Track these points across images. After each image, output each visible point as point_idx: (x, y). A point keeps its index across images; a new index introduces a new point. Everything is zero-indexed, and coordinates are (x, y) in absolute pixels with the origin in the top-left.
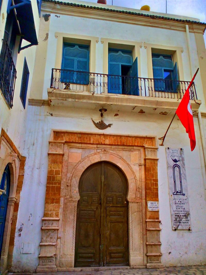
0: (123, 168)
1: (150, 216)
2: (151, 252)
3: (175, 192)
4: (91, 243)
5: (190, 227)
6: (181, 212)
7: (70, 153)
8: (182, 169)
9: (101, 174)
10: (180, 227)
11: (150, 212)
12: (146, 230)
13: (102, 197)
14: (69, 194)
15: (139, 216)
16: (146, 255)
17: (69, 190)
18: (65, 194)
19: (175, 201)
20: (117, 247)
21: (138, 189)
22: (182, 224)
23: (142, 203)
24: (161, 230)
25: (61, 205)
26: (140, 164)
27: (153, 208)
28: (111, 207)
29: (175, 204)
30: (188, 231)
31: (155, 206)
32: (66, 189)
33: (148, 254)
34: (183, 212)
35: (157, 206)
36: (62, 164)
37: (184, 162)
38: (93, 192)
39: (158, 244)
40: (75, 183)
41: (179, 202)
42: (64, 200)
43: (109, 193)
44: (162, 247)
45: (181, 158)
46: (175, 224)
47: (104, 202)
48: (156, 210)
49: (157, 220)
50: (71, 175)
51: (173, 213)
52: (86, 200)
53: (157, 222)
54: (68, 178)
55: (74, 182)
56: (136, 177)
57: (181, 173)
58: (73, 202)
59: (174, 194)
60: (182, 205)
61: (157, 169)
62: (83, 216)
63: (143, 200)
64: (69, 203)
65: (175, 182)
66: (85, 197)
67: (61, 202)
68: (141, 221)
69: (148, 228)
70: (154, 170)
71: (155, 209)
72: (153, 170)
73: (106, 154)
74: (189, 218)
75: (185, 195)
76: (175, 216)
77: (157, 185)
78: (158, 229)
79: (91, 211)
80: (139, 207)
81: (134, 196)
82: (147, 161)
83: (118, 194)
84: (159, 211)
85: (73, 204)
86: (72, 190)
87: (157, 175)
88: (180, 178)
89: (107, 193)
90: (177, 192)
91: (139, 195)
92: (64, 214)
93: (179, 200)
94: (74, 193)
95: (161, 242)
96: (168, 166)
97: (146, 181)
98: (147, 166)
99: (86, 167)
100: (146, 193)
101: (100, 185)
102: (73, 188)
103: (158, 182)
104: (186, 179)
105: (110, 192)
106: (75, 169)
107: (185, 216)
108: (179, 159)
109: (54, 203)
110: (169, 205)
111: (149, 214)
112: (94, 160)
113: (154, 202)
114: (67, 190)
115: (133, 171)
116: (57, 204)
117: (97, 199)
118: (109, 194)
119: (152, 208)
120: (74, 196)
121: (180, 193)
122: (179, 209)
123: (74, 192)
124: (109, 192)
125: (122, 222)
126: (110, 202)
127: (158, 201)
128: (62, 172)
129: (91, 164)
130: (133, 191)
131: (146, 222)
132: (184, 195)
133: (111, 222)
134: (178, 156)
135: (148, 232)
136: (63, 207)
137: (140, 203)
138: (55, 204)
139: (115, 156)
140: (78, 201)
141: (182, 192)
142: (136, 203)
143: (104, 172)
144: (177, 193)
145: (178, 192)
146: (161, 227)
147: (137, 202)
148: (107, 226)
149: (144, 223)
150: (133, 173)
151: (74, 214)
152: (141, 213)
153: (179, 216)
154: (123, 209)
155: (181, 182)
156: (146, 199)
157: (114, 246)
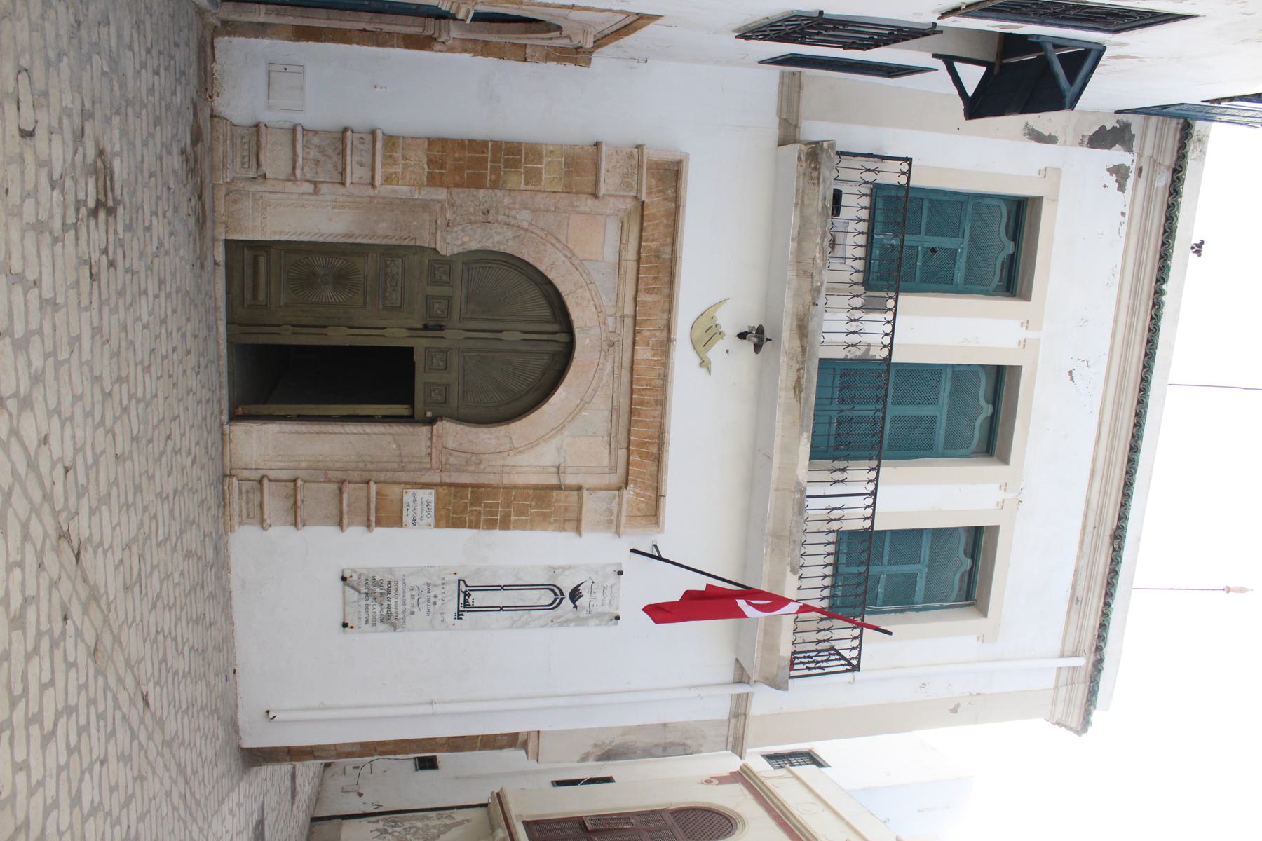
6: (400, 600)
12: (343, 482)
16: (263, 477)
19: (435, 586)
22: (363, 603)
29: (429, 585)
33: (265, 481)
34: (400, 608)
40: (497, 238)
42: (439, 201)
45: (583, 614)
46: (363, 578)
48: (407, 519)
50: (525, 225)
51: (398, 576)
53: (369, 520)
54: (513, 213)
55: (499, 234)
60: (424, 606)
65: (502, 588)
67: (432, 189)
68: (370, 466)
69: (348, 488)
74: (381, 626)
82: (575, 493)
88: (516, 608)
90: (467, 594)
92: (391, 203)
98: (555, 493)
100: (464, 486)
102: (479, 231)
107: (389, 615)
112: (577, 304)
122: (413, 596)
127: (437, 526)
131: (368, 483)
135: (334, 486)
137: (428, 466)
147: (430, 454)
152: (395, 465)
156: (441, 485)
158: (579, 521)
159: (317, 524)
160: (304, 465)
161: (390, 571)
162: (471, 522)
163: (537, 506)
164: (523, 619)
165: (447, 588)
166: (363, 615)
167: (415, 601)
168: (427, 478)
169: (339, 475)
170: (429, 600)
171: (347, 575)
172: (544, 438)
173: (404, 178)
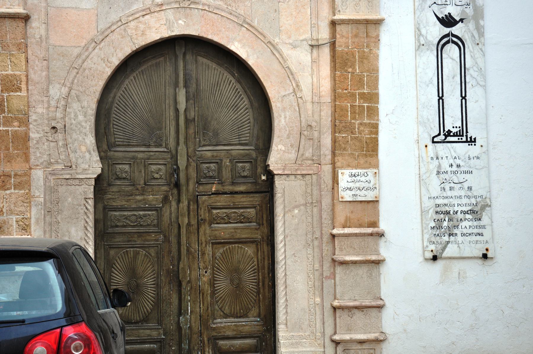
0: (251, 57)
1: (347, 217)
2: (349, 330)
3: (439, 134)
4: (150, 311)
5: (487, 250)
6: (456, 202)
7: (51, 11)
8: (471, 52)
9: (176, 85)
10: (451, 251)
11: (348, 204)
12: (334, 261)
13: (182, 163)
14: (62, 157)
15: (310, 220)
16: (333, 341)
17: (60, 144)
18: (45, 157)
19: (439, 166)
20: (236, 320)
21: (306, 132)
22: (459, 238)
23: (319, 178)
24: (383, 261)
25: (37, 194)
26: (313, 43)
27: (358, 192)
28: (213, 194)
29: (438, 173)
30: (480, 262)
31: (366, 185)
32: (50, 139)
33: (337, 337)
34: (465, 201)
35: (372, 183)
36: (26, 52)
37: (482, 22)
38: (149, 146)
39: (374, 304)
40: (81, 118)
41: (451, 165)
42: (46, 179)
43: (204, 149)
44: (387, 315)
45: (469, 11)
46: (433, 239)
47: (188, 180)
48: (370, 196)
49: (370, 230)
50: (65, 90)
51: (429, 204)
52: (124, 175)
53: (371, 235)
54: (53, 103)
55: (76, 116)
56: (301, 91)
57: (467, 66)
58: (77, 182)
59: (435, 140)
60: (461, 177)
61: (378, 56)
62: (117, 226)
63: (323, 167)
64: (64, 187)
65: (441, 98)
66: (121, 166)
67: (33, 184)
68: (318, 234)
69: (339, 257)
70: (365, 61)
71: (363, 192)
72: (361, 62)
73: (188, 11)
74: (485, 220)
75: (475, 141)
76: (437, 212)
77: (373, 112)
78: (374, 258)
79: (144, 209)
80: (309, 191)
81: (293, 156)
82: (338, 28)
83: (237, 150)
84: (377, 201)
85: (80, 189)
86: (73, 144)
87: (377, 79)
88: (463, 83)
89: (200, 149)
90: (448, 134)
91: (311, 150)
92: (50, 224)
93: (451, 161)
94: (79, 153)
95: (383, 300)
96: (419, 42)
97: (335, 101)
98: (338, 49)
99: (116, 62)
100: (334, 141)
101: (173, 123)
102: (74, 136)
103: (378, 102)
104: (484, 87)
105: (209, 145)
106: (76, 70)
107: (472, 212)
108: (463, 12)
109: (8, 189)
110: (418, 179)
111: (341, 214)
112: (143, 34)
113: (362, 171)
114: (52, 144)
115: (288, 67)
116: (23, 191)
117: (166, 171)
118: (207, 151)
119: (353, 192)
120: (80, 161)
121: (457, 136)
122: (451, 189)
123: (80, 149)
124: (204, 146)
125: (253, 242)
126: (211, 177)
127: (377, 166)
128: (30, 82)
129: (134, 49)
130: (288, 137)
131: (333, 236)
132: (471, 141)
133: (217, 243)
134: (460, 4)
135: (339, 270)
136: (42, 200)
138: (12, 191)
139: (222, 16)
140: (98, 179)
141: (467, 132)
142: (298, 176)
143: (185, 75)
144: (446, 136)
145: (449, 131)
146: (385, 251)
147: (303, 175)
148: (203, 254)
149: (325, 240)
150: (290, 74)
151: (83, 222)
152: (315, 210)
153: (451, 213)
154: (256, 199)
155: (464, 98)
156: (333, 163)
157: (226, 316)
158: (367, 22)
159: (378, 286)
160: (318, 300)
161: (423, 212)
162: (371, 133)
163: (353, 66)
164: (475, 74)
165: (441, 154)
166: (474, 238)
167: (457, 186)
168: (327, 178)
169: (327, 265)
170: (455, 173)
171: (430, 255)
172: (282, 61)
173: (22, 213)
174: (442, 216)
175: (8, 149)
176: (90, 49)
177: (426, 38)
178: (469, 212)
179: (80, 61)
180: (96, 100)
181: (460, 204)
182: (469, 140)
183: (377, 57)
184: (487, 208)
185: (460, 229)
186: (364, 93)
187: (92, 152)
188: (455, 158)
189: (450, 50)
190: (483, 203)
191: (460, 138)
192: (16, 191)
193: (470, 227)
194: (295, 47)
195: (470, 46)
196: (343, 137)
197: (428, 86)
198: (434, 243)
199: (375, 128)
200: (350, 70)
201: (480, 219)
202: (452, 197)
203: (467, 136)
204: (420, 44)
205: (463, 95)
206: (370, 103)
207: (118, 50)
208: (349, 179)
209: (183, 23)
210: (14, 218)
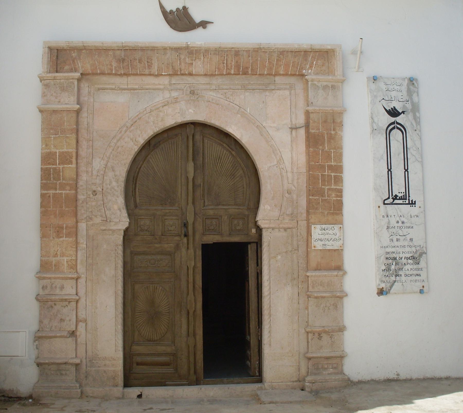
3: (389, 198)
5: (423, 287)
6: (400, 250)
8: (411, 136)
19: (389, 222)
22: (403, 278)
27: (327, 243)
29: (388, 228)
31: (334, 237)
33: (310, 355)
34: (408, 249)
40: (114, 184)
45: (409, 106)
46: (384, 279)
48: (336, 245)
55: (111, 182)
59: (386, 202)
60: (405, 231)
65: (389, 170)
70: (332, 141)
72: (329, 142)
74: (422, 264)
75: (415, 204)
83: (233, 210)
90: (395, 198)
93: (398, 219)
96: (373, 127)
99: (142, 141)
100: (309, 202)
103: (342, 172)
107: (413, 258)
108: (404, 106)
109: (61, 237)
119: (323, 243)
121: (402, 199)
122: (397, 240)
127: (341, 223)
132: (412, 204)
134: (401, 100)
136: (85, 246)
138: (64, 239)
140: (126, 231)
141: (409, 197)
144: (394, 199)
145: (396, 196)
153: (398, 259)
155: (406, 170)
156: (308, 220)
161: (378, 258)
162: (337, 196)
163: (323, 144)
166: (414, 278)
170: (400, 228)
174: (391, 261)
175: (62, 207)
176: (123, 132)
177: (378, 124)
178: (411, 258)
179: (115, 141)
180: (126, 170)
181: (404, 253)
182: (411, 202)
183: (341, 138)
184: (424, 255)
185: (404, 271)
186: (332, 165)
187: (122, 209)
188: (401, 216)
189: (395, 134)
190: (421, 251)
191: (404, 201)
192: (67, 239)
193: (411, 269)
194: (278, 130)
195: (410, 131)
196: (315, 199)
197: (380, 160)
198: (384, 282)
199: (340, 192)
200: (321, 147)
201: (418, 264)
202: (398, 247)
203: (409, 199)
204: (374, 129)
205: (406, 168)
206: (336, 173)
207: (143, 132)
208: (320, 233)
209: (192, 112)
210: (65, 259)
